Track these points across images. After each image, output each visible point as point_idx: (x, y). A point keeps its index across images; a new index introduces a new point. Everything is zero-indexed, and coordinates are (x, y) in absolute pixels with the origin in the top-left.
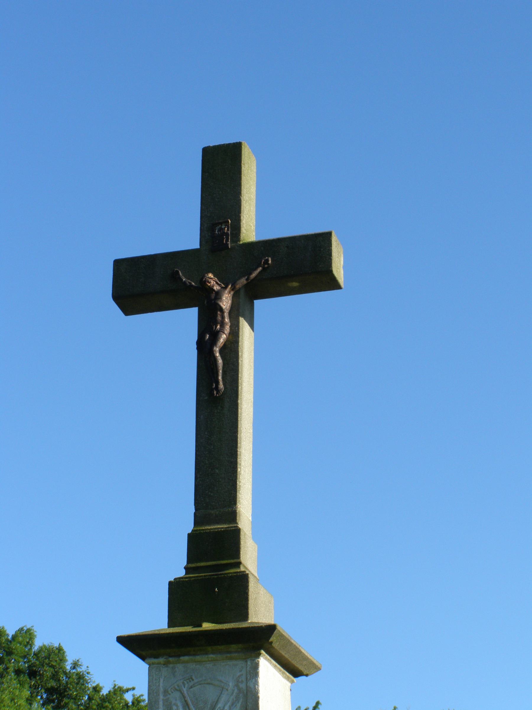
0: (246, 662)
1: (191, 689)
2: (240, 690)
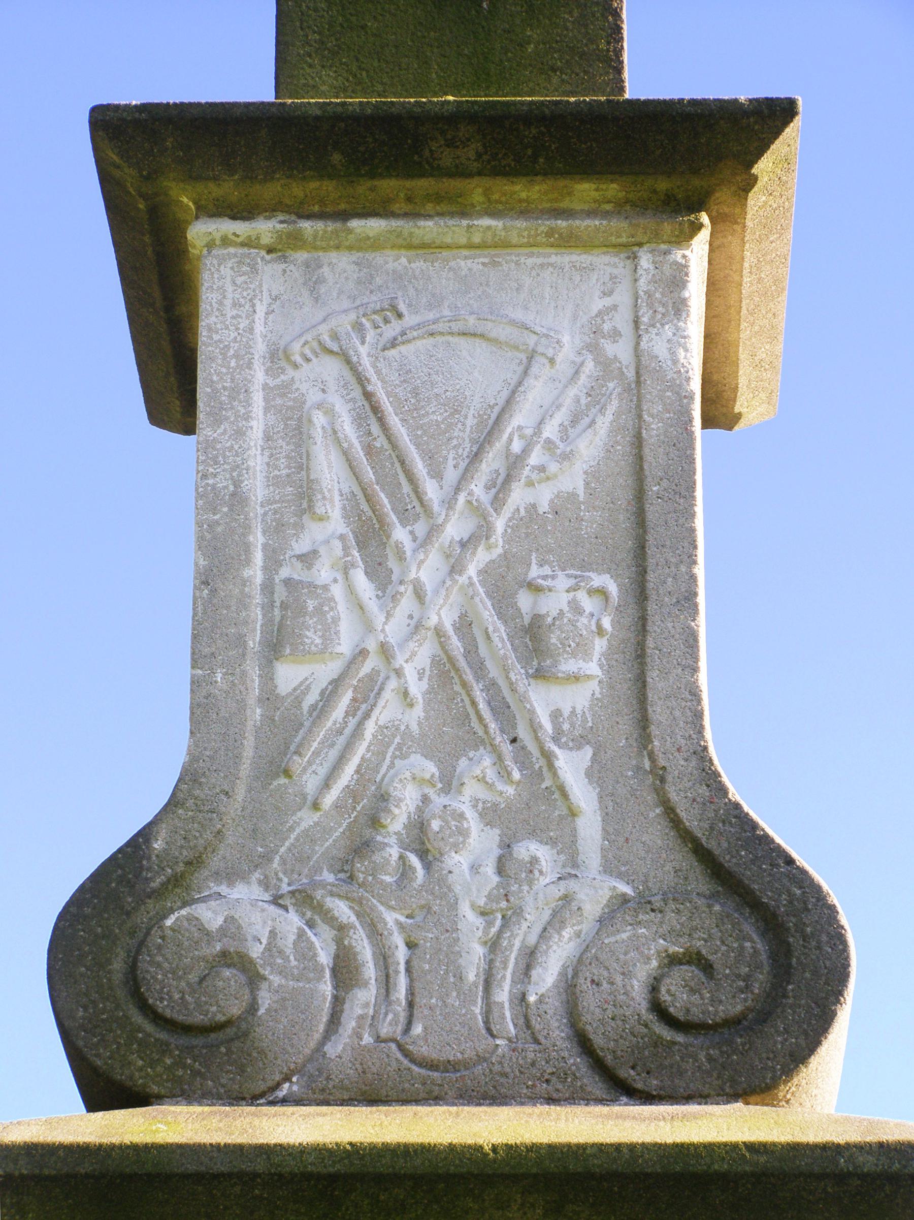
0: (634, 257)
1: (393, 352)
2: (606, 365)
